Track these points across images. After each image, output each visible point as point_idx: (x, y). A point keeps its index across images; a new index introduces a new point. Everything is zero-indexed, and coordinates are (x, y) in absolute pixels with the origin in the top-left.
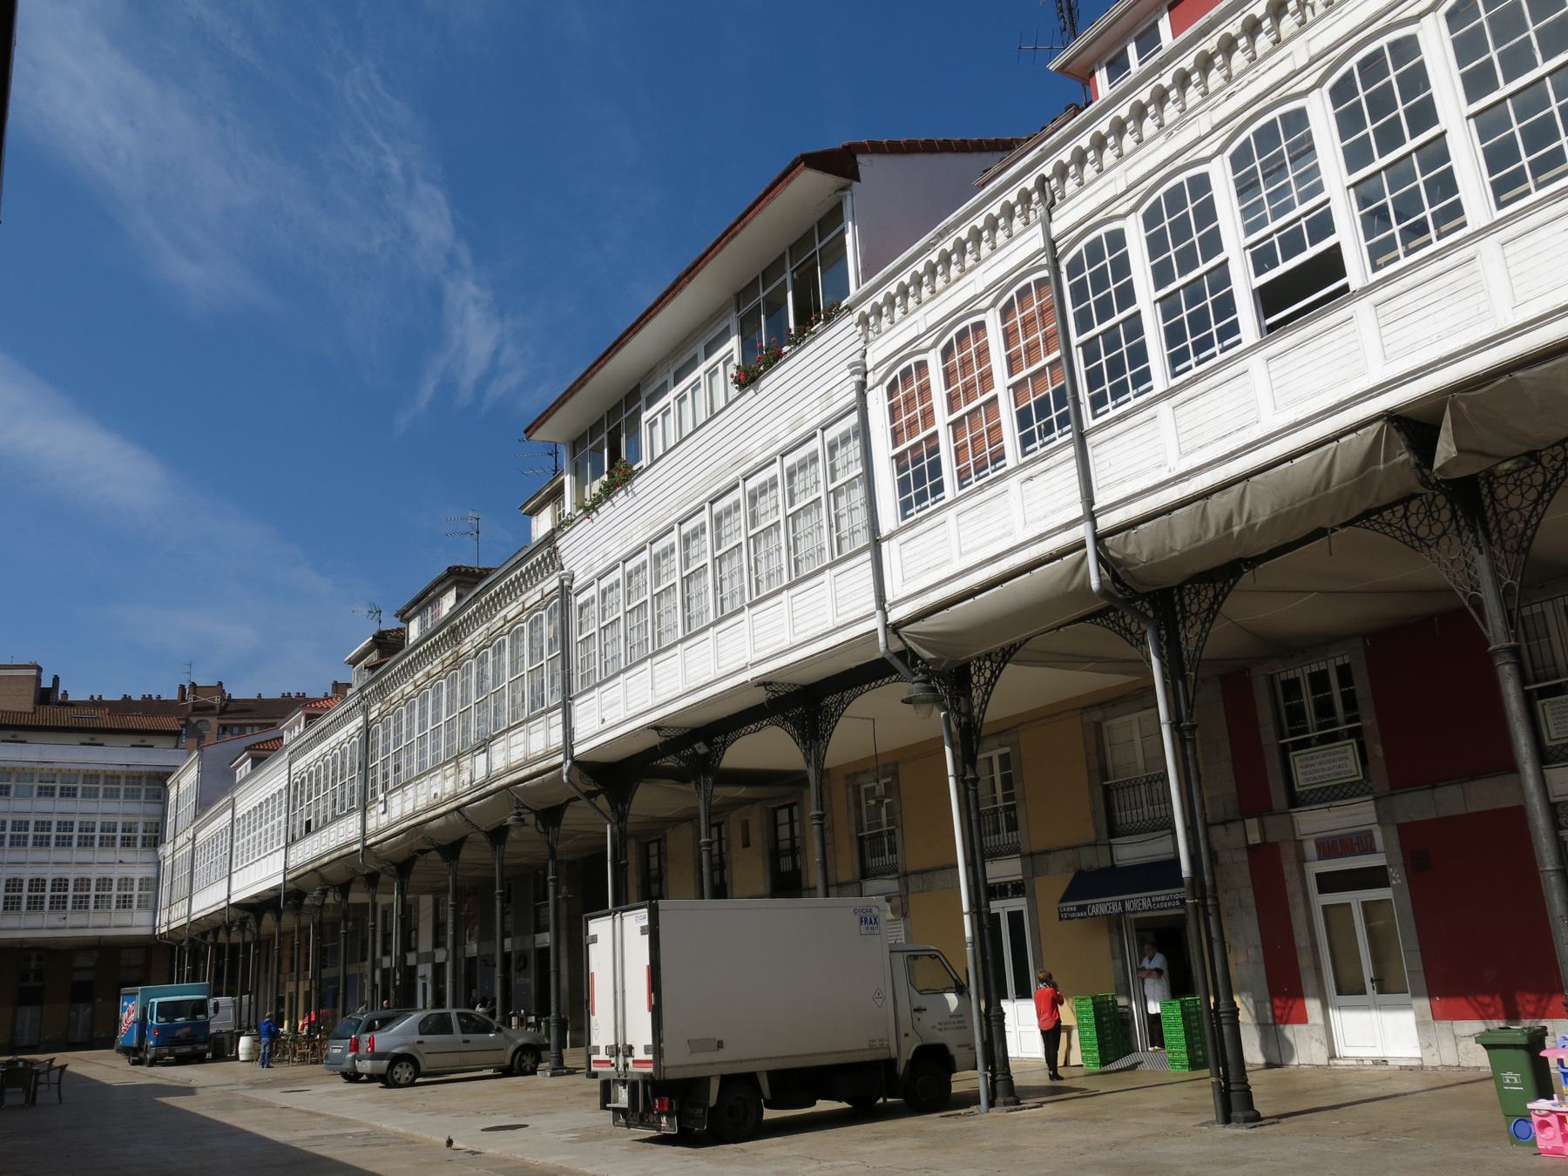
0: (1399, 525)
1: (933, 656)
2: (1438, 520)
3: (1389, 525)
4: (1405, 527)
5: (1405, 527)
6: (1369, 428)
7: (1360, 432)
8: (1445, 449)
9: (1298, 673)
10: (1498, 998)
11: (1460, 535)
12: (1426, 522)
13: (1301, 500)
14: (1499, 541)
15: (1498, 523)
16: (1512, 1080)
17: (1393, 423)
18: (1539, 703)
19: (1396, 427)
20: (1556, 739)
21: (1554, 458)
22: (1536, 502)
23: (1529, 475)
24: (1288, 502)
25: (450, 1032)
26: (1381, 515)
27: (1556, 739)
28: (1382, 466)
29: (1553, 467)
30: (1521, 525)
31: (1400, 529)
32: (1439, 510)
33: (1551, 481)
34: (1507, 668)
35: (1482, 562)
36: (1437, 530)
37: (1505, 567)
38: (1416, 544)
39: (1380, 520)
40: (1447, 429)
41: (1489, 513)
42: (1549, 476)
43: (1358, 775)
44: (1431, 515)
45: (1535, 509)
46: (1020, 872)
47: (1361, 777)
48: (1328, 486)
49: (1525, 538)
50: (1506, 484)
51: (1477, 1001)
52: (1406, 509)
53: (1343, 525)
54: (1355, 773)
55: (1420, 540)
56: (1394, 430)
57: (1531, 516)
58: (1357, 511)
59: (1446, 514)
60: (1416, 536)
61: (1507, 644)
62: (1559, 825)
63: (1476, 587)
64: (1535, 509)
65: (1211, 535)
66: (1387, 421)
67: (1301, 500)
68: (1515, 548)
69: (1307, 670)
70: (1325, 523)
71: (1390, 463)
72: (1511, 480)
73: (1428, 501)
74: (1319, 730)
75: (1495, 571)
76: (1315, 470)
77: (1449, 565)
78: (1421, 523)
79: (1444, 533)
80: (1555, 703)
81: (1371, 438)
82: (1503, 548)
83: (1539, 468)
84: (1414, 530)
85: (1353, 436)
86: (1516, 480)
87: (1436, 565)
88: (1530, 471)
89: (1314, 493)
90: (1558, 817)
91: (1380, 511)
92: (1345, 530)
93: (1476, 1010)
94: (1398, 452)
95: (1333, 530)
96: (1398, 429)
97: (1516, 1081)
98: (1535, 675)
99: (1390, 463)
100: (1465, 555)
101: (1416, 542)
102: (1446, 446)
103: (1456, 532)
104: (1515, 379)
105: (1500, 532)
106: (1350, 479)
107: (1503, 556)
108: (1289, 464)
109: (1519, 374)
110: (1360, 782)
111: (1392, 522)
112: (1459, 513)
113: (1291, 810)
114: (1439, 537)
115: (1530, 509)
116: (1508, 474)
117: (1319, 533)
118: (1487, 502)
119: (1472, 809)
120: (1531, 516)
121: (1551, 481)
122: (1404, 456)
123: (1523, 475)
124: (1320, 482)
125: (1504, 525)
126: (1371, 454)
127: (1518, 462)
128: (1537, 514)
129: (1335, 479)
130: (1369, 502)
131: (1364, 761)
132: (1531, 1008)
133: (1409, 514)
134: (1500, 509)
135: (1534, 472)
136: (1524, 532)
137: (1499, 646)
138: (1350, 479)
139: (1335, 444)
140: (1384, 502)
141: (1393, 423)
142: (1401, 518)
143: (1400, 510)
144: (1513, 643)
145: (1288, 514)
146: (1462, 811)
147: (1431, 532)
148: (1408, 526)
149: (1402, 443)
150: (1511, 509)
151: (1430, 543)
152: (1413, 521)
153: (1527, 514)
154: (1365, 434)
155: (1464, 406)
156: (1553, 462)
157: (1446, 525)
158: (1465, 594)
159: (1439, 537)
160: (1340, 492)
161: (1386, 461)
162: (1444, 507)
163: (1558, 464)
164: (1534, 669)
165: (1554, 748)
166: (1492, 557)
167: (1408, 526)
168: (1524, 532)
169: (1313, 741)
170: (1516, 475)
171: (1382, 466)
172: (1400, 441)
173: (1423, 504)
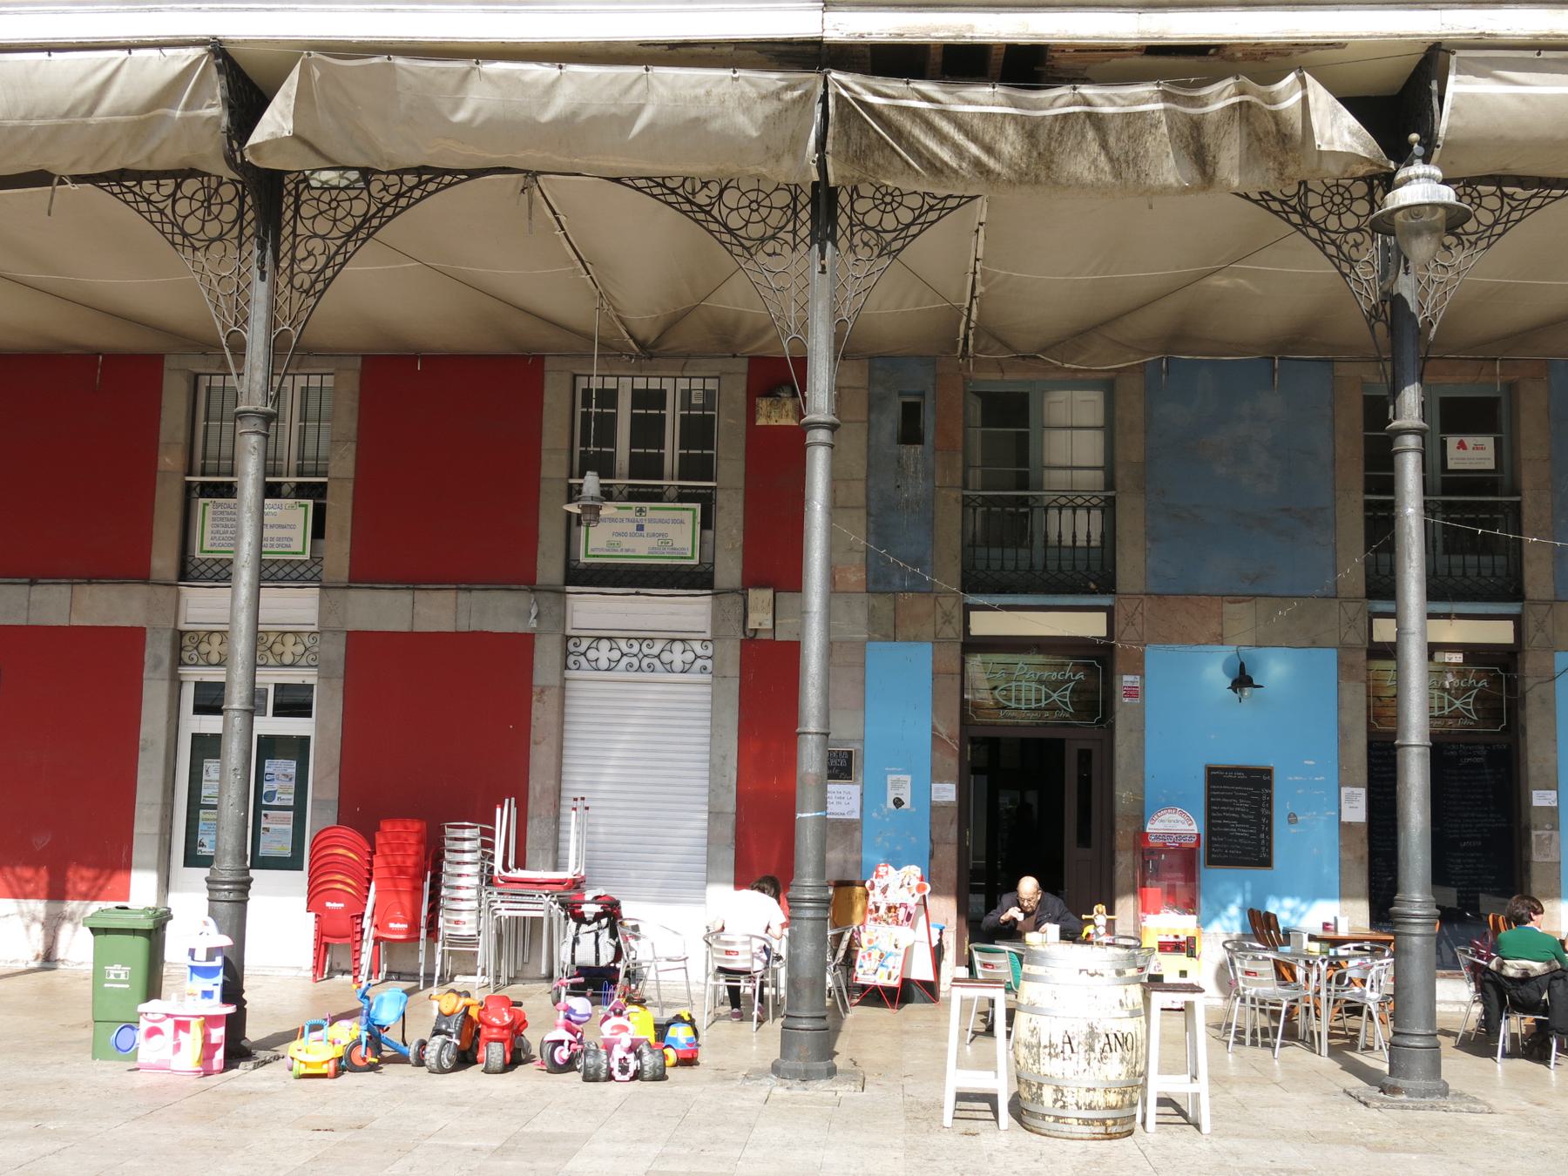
0: (161, 206)
1: (630, 137)
2: (217, 217)
3: (149, 201)
4: (168, 211)
5: (168, 211)
6: (184, 52)
7: (165, 51)
8: (276, 122)
9: (667, 384)
10: (43, 872)
11: (241, 246)
12: (200, 213)
13: (43, 117)
14: (288, 271)
15: (294, 247)
16: (117, 976)
17: (217, 57)
18: (202, 501)
19: (218, 66)
20: (208, 552)
21: (386, 188)
22: (349, 235)
23: (350, 200)
24: (21, 113)
25: (477, 952)
26: (140, 183)
27: (208, 552)
28: (178, 113)
29: (381, 199)
30: (322, 260)
31: (161, 212)
32: (222, 204)
33: (374, 216)
34: (254, 440)
35: (260, 291)
36: (213, 229)
37: (286, 308)
38: (178, 239)
39: (137, 189)
40: (288, 96)
41: (287, 231)
42: (373, 209)
43: (303, 553)
44: (209, 207)
45: (345, 243)
46: (315, 621)
47: (307, 556)
48: (90, 112)
49: (322, 278)
50: (318, 200)
51: (14, 874)
52: (178, 186)
53: (78, 179)
54: (689, 554)
55: (185, 235)
56: (214, 70)
57: (336, 253)
58: (113, 165)
59: (230, 213)
60: (182, 229)
61: (262, 409)
62: (181, 659)
63: (804, 326)
64: (345, 243)
65: (546, 117)
66: (210, 51)
67: (43, 117)
68: (306, 286)
69: (683, 384)
70: (59, 165)
71: (191, 113)
72: (326, 197)
73: (209, 187)
74: (680, 479)
75: (273, 307)
76: (83, 80)
77: (215, 282)
78: (193, 212)
79: (220, 238)
80: (220, 505)
81: (179, 66)
82: (291, 281)
83: (365, 195)
84: (180, 220)
85: (154, 53)
86: (332, 200)
87: (197, 277)
88: (353, 193)
89: (66, 115)
90: (181, 649)
91: (140, 176)
92: (77, 187)
93: (9, 886)
94: (209, 102)
95: (62, 182)
96: (220, 69)
97: (123, 977)
98: (204, 466)
99: (191, 113)
100: (240, 276)
101: (181, 238)
102: (279, 118)
103: (236, 242)
104: (393, 65)
105: (293, 259)
106: (127, 113)
107: (287, 293)
108: (44, 55)
109: (399, 61)
110: (302, 562)
111: (152, 198)
112: (250, 215)
113: (569, 589)
114: (212, 241)
115: (339, 242)
116: (326, 188)
117: (41, 178)
118: (289, 214)
119: (76, 622)
120: (336, 253)
121: (374, 216)
122: (214, 109)
123: (343, 196)
124: (81, 101)
125: (300, 253)
126: (170, 91)
127: (341, 177)
128: (346, 253)
129: (106, 105)
130: (136, 160)
131: (318, 531)
132: (83, 887)
133: (179, 195)
134: (300, 229)
135: (356, 198)
136: (322, 271)
137: (251, 408)
138: (127, 113)
139: (124, 54)
140: (157, 165)
141: (217, 57)
142: (169, 196)
143: (168, 186)
144: (269, 408)
145: (14, 130)
146: (64, 622)
147: (202, 229)
148: (174, 211)
149: (218, 91)
150: (315, 235)
151: (197, 244)
152: (183, 207)
153: (333, 249)
154: (173, 57)
155: (317, 74)
156: (384, 193)
157: (227, 227)
158: (225, 326)
159: (212, 241)
160: (105, 128)
161: (187, 107)
162: (229, 203)
163: (387, 199)
164: (204, 457)
165: (203, 562)
166: (274, 289)
167: (174, 211)
168: (322, 271)
169: (285, 489)
170: (334, 192)
171: (178, 113)
172: (217, 88)
173: (204, 188)
